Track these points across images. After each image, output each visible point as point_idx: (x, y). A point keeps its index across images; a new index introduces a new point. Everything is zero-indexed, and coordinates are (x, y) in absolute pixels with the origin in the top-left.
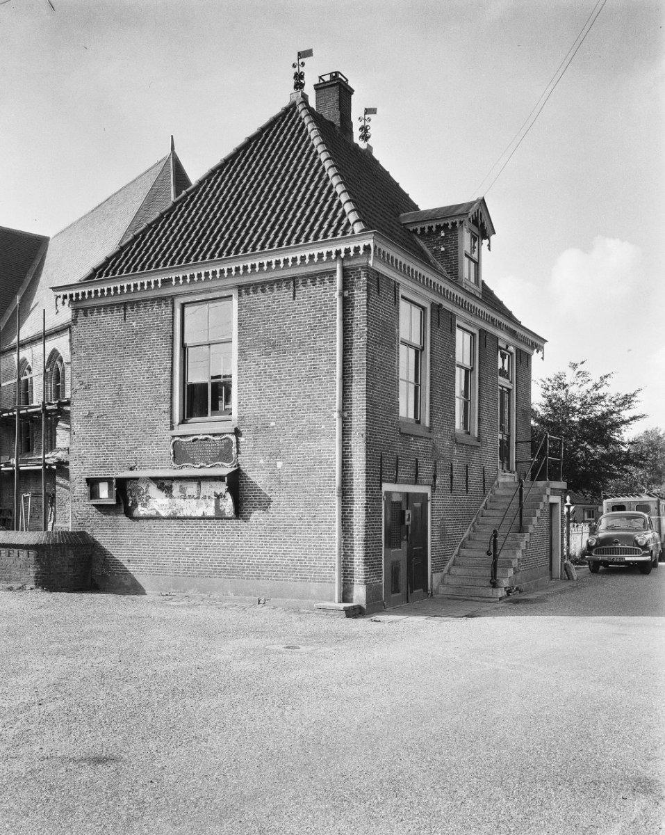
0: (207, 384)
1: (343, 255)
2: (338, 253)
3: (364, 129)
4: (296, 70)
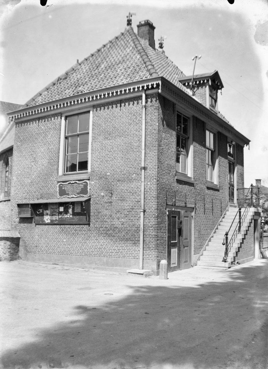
0: (88, 170)
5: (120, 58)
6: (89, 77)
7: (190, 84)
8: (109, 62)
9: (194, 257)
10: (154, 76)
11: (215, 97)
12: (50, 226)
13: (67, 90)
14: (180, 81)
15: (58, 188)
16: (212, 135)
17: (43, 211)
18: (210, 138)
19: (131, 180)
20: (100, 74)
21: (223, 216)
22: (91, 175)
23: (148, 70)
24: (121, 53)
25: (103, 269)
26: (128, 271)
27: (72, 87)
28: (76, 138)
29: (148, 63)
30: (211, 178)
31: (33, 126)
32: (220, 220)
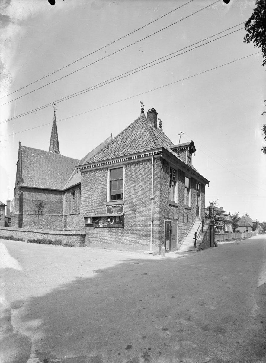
1: (154, 154)
2: (152, 153)
3: (160, 125)
4: (142, 107)
5: (139, 135)
6: (122, 146)
7: (177, 150)
8: (132, 137)
9: (178, 246)
10: (158, 146)
11: (190, 157)
12: (103, 229)
13: (110, 154)
14: (171, 149)
15: (107, 209)
16: (188, 179)
17: (98, 221)
18: (187, 180)
19: (145, 205)
20: (128, 145)
21: (193, 224)
22: (125, 202)
23: (155, 143)
24: (139, 132)
25: (131, 251)
26: (144, 252)
27: (112, 152)
28: (116, 182)
29: (155, 139)
30: (187, 204)
31: (92, 174)
32: (184, 238)
